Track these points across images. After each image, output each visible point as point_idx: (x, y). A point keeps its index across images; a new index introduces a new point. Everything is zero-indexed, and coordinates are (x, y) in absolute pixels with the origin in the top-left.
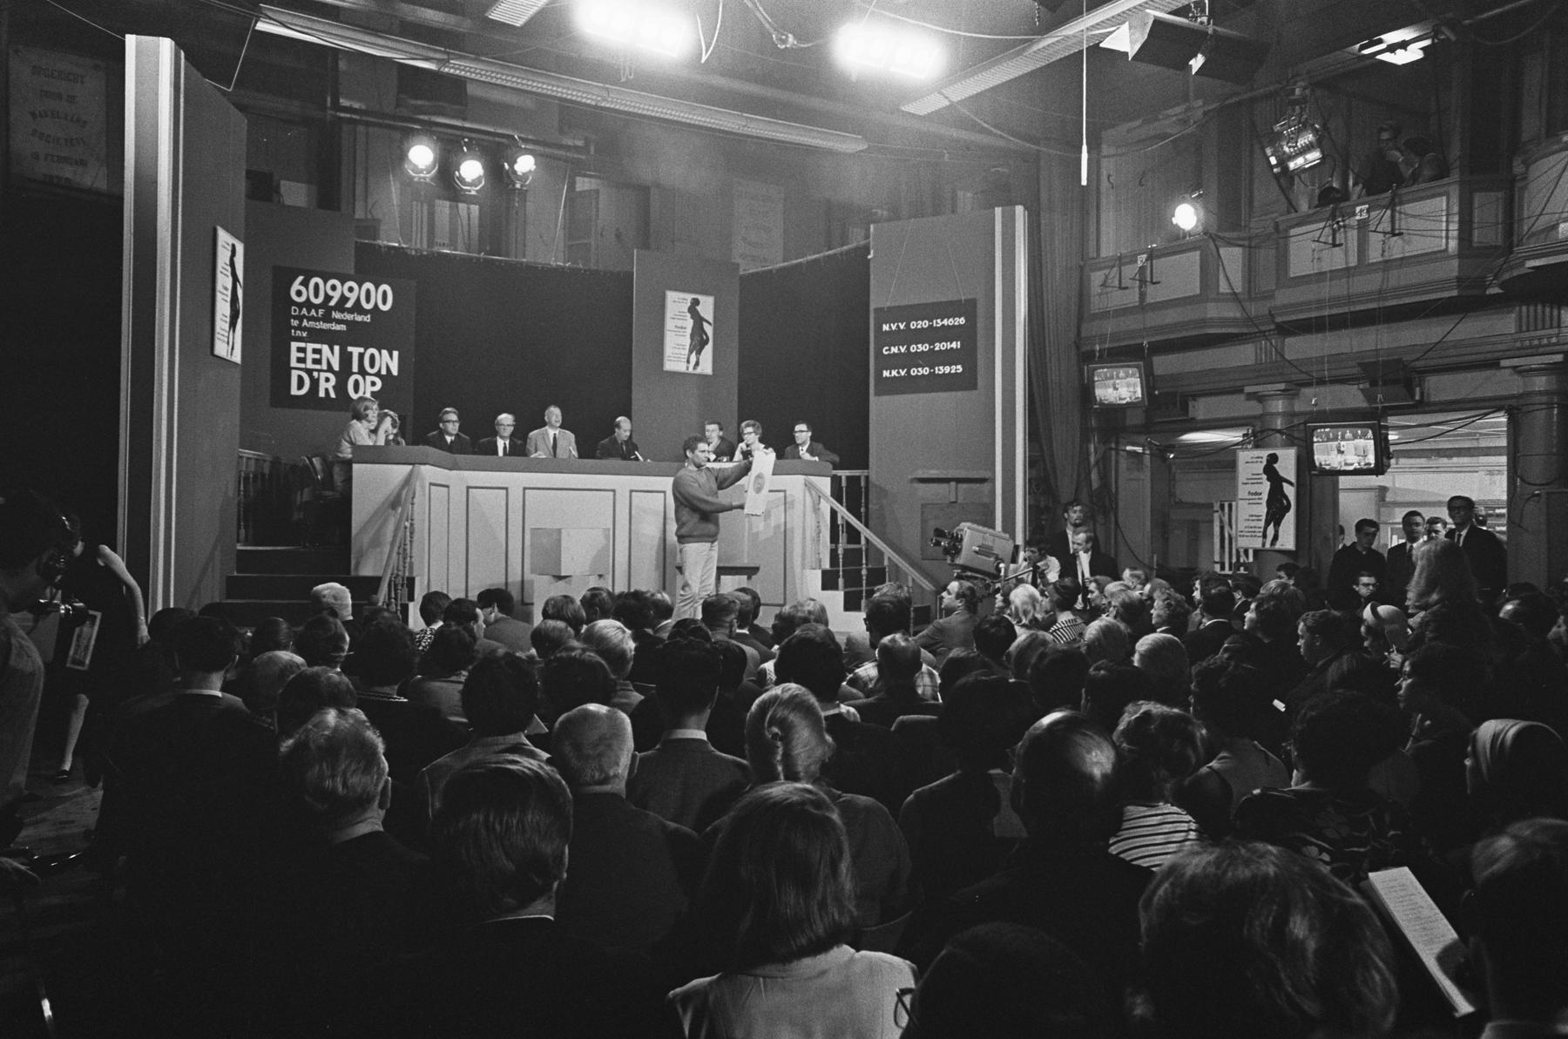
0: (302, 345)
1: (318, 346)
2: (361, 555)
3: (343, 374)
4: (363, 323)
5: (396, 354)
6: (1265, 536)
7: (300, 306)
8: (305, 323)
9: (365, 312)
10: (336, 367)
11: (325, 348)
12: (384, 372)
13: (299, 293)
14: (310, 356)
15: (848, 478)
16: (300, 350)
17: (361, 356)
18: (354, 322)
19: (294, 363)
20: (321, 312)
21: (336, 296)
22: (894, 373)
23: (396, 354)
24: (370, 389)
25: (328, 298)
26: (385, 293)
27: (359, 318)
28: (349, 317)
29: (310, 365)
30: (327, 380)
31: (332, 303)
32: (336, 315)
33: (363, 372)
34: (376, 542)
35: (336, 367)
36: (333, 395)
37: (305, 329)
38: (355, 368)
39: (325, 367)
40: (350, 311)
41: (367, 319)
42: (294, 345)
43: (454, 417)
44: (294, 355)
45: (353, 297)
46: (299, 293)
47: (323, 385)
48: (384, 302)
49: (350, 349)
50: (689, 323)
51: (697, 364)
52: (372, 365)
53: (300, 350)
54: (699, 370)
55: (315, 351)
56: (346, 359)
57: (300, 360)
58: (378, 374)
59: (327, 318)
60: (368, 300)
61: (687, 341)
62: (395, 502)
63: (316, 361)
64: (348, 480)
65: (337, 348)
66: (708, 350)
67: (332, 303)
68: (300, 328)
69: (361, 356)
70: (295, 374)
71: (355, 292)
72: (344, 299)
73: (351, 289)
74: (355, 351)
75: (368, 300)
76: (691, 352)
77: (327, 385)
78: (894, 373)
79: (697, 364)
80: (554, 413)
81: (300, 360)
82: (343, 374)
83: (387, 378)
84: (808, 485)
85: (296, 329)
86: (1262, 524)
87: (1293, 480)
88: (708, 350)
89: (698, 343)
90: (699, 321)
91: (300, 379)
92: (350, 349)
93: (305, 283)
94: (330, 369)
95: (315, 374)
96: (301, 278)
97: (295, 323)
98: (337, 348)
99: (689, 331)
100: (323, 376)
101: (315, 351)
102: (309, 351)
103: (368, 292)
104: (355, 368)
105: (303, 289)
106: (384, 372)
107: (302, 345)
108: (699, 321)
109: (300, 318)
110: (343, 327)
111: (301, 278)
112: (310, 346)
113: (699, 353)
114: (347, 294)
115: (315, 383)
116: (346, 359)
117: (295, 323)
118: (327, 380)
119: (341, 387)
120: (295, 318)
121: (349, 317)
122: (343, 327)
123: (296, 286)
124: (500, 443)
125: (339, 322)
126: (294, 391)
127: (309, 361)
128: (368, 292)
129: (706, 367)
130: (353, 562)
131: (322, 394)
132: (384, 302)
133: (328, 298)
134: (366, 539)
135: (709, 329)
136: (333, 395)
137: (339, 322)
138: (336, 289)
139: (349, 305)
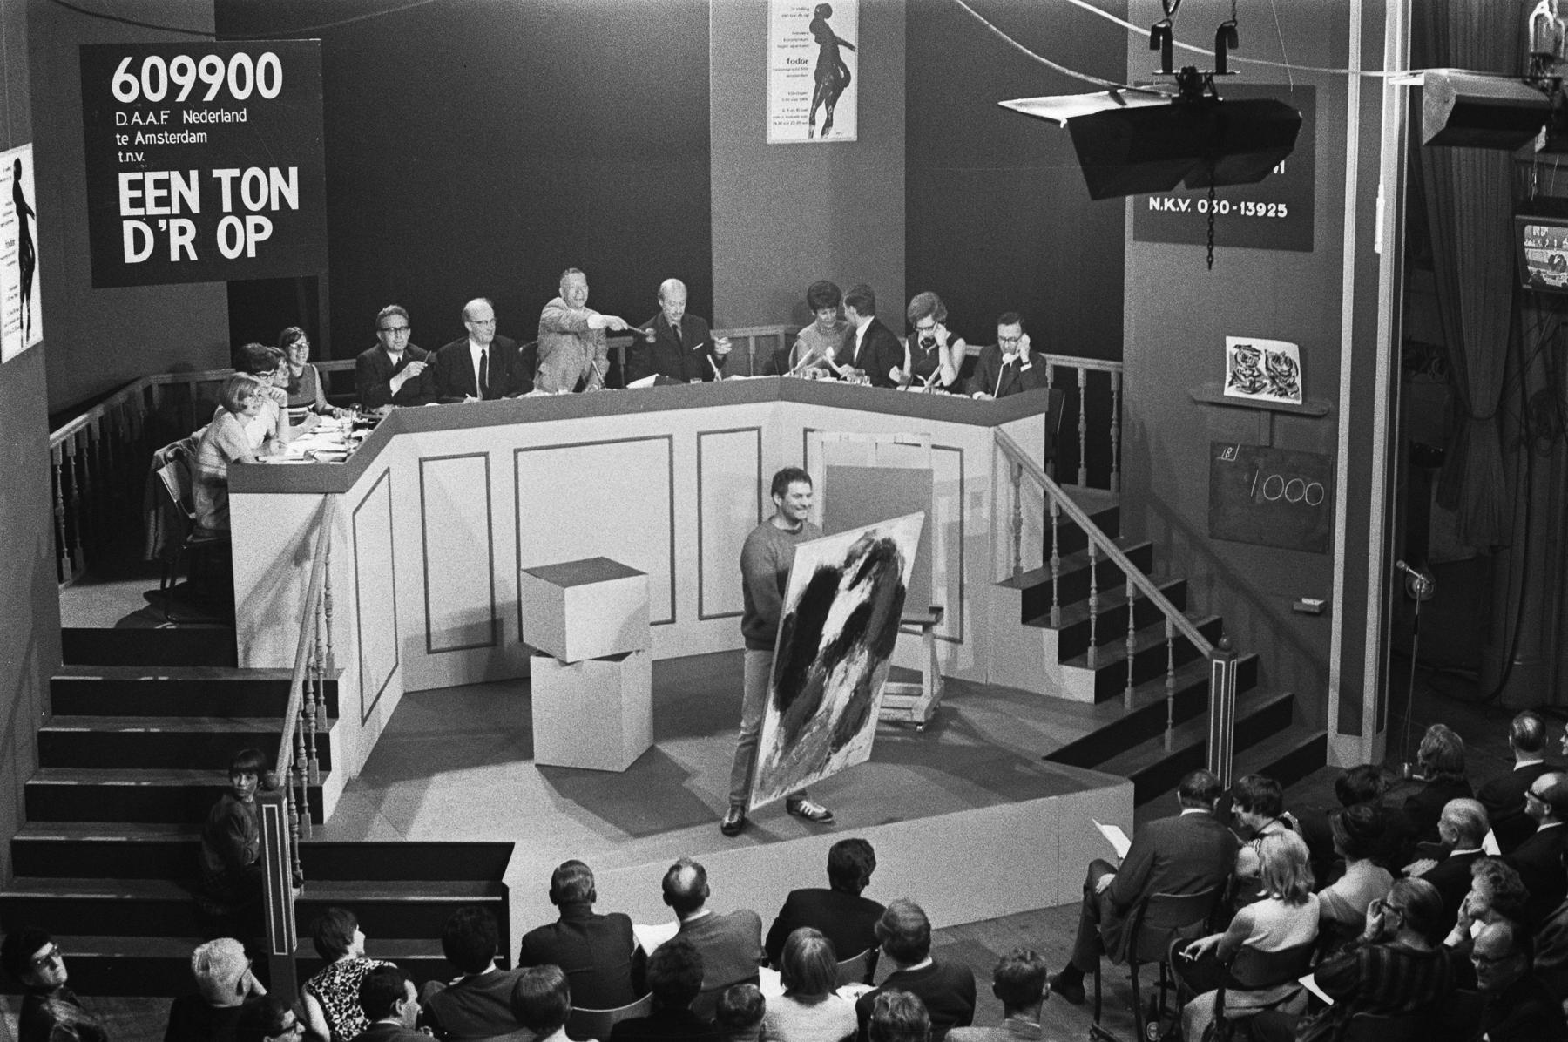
0: (137, 176)
1: (163, 175)
2: (252, 634)
3: (207, 219)
4: (236, 124)
5: (293, 171)
6: (812, 122)
7: (129, 108)
8: (139, 138)
9: (236, 105)
10: (195, 208)
11: (176, 177)
12: (275, 206)
13: (126, 87)
14: (152, 193)
15: (1090, 373)
16: (133, 185)
17: (236, 183)
18: (220, 124)
19: (125, 210)
20: (164, 115)
21: (187, 82)
22: (1168, 204)
23: (293, 171)
24: (254, 238)
25: (174, 89)
26: (269, 66)
27: (228, 118)
28: (212, 117)
29: (152, 210)
30: (182, 231)
31: (182, 97)
32: (191, 117)
33: (240, 211)
34: (273, 617)
35: (195, 208)
36: (193, 256)
37: (139, 148)
38: (227, 206)
39: (176, 210)
40: (213, 106)
41: (242, 117)
42: (124, 178)
43: (397, 321)
44: (125, 194)
45: (216, 81)
46: (126, 87)
47: (175, 241)
48: (269, 85)
49: (216, 173)
50: (813, 51)
51: (829, 123)
52: (255, 197)
53: (133, 185)
54: (832, 136)
55: (159, 184)
56: (210, 191)
57: (137, 203)
58: (266, 211)
59: (176, 125)
60: (241, 86)
61: (810, 84)
62: (299, 554)
63: (160, 202)
64: (222, 513)
65: (194, 174)
66: (848, 99)
67: (182, 97)
68: (131, 147)
69: (236, 183)
70: (128, 227)
71: (212, 73)
72: (200, 87)
73: (211, 69)
74: (225, 175)
75: (241, 86)
76: (816, 103)
77: (182, 240)
78: (1168, 204)
79: (829, 123)
80: (575, 282)
81: (137, 203)
82: (207, 219)
83: (282, 216)
84: (1001, 443)
85: (125, 149)
86: (809, 104)
87: (853, 42)
88: (848, 99)
89: (829, 84)
90: (829, 44)
91: (138, 235)
92: (216, 173)
93: (134, 69)
94: (185, 211)
95: (162, 223)
96: (127, 61)
97: (122, 140)
98: (194, 174)
99: (813, 65)
100: (175, 224)
101: (159, 184)
102: (149, 185)
103: (241, 68)
104: (227, 206)
105: (131, 79)
106: (275, 206)
107: (137, 176)
108: (829, 44)
109: (131, 130)
110: (202, 137)
111: (127, 61)
112: (151, 177)
113: (832, 103)
114: (205, 78)
115: (162, 239)
116: (210, 191)
117: (122, 140)
118: (182, 231)
119: (205, 240)
120: (122, 131)
121: (212, 117)
122: (202, 137)
123: (120, 76)
124: (476, 351)
125: (195, 128)
126: (130, 257)
127: (150, 202)
128: (241, 68)
129: (845, 122)
130: (240, 648)
131: (175, 256)
132: (269, 85)
133: (174, 89)
134: (258, 612)
135: (849, 58)
136: (193, 256)
137: (195, 128)
138: (185, 72)
139: (210, 96)
